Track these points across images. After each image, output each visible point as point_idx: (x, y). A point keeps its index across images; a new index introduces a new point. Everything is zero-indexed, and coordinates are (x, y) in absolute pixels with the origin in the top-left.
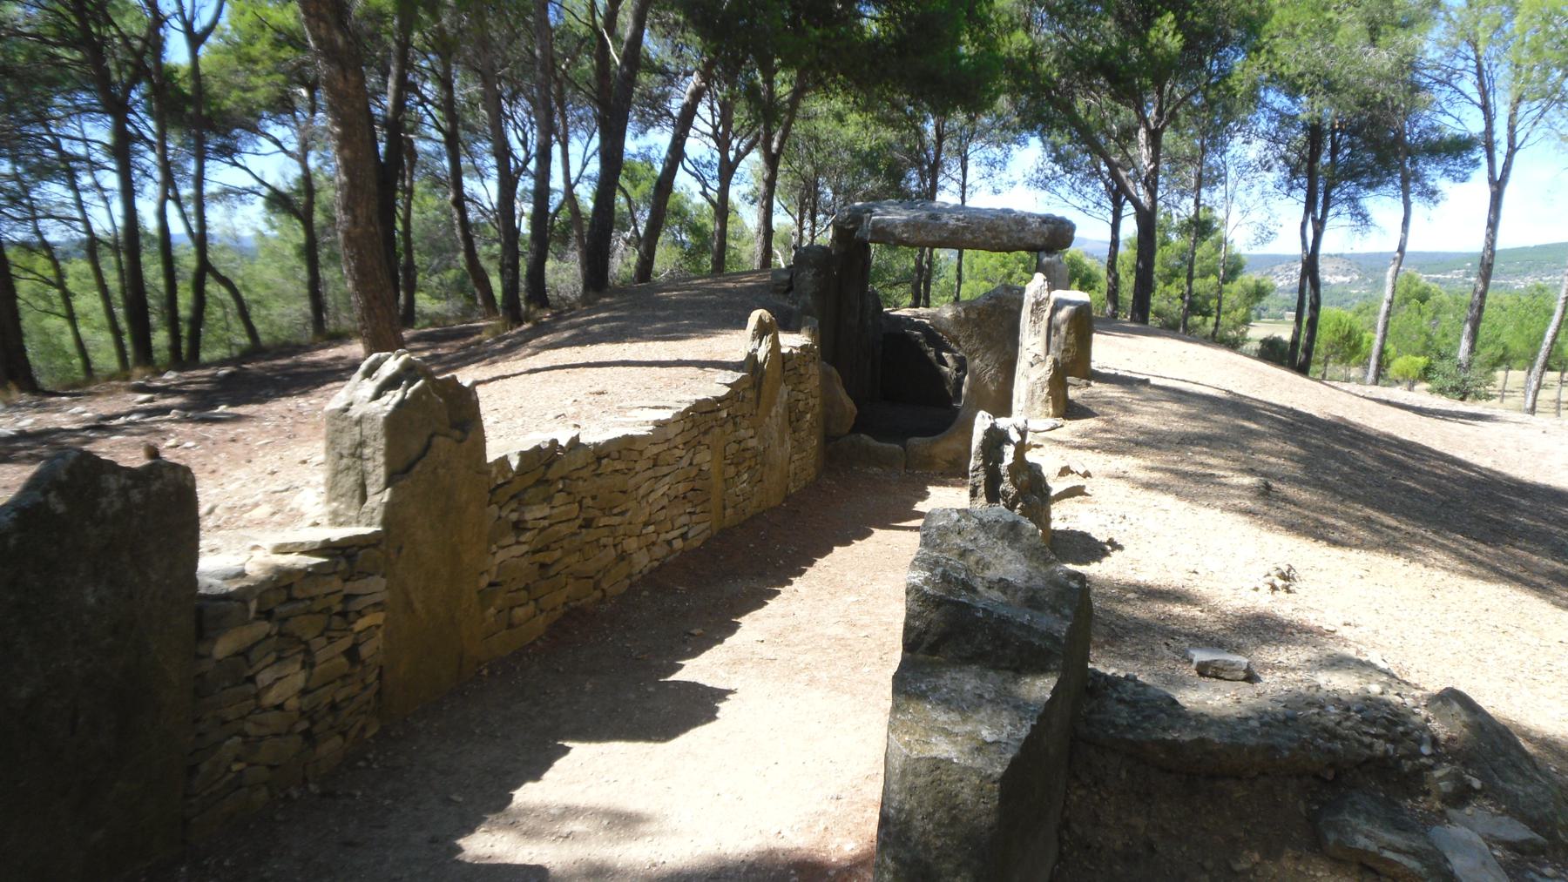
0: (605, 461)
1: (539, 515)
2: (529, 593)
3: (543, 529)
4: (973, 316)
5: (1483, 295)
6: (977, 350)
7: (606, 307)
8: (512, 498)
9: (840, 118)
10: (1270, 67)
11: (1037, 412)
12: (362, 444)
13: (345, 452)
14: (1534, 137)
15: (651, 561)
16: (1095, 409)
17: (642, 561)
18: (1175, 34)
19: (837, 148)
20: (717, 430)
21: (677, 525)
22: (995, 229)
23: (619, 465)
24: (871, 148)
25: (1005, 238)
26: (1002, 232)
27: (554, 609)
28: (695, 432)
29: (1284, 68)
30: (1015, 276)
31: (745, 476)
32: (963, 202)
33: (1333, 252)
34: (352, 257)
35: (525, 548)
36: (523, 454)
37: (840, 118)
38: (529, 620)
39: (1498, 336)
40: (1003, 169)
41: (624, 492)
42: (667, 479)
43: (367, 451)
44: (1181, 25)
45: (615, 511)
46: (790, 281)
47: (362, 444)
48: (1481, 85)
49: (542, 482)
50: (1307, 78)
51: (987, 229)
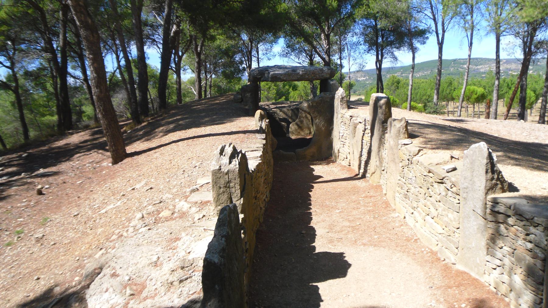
4: (315, 104)
5: (439, 81)
6: (317, 116)
10: (367, 10)
12: (229, 182)
13: (222, 186)
14: (449, 27)
22: (315, 73)
24: (226, 48)
26: (317, 74)
30: (271, 88)
34: (101, 106)
43: (232, 185)
47: (229, 182)
48: (433, 12)
51: (312, 74)
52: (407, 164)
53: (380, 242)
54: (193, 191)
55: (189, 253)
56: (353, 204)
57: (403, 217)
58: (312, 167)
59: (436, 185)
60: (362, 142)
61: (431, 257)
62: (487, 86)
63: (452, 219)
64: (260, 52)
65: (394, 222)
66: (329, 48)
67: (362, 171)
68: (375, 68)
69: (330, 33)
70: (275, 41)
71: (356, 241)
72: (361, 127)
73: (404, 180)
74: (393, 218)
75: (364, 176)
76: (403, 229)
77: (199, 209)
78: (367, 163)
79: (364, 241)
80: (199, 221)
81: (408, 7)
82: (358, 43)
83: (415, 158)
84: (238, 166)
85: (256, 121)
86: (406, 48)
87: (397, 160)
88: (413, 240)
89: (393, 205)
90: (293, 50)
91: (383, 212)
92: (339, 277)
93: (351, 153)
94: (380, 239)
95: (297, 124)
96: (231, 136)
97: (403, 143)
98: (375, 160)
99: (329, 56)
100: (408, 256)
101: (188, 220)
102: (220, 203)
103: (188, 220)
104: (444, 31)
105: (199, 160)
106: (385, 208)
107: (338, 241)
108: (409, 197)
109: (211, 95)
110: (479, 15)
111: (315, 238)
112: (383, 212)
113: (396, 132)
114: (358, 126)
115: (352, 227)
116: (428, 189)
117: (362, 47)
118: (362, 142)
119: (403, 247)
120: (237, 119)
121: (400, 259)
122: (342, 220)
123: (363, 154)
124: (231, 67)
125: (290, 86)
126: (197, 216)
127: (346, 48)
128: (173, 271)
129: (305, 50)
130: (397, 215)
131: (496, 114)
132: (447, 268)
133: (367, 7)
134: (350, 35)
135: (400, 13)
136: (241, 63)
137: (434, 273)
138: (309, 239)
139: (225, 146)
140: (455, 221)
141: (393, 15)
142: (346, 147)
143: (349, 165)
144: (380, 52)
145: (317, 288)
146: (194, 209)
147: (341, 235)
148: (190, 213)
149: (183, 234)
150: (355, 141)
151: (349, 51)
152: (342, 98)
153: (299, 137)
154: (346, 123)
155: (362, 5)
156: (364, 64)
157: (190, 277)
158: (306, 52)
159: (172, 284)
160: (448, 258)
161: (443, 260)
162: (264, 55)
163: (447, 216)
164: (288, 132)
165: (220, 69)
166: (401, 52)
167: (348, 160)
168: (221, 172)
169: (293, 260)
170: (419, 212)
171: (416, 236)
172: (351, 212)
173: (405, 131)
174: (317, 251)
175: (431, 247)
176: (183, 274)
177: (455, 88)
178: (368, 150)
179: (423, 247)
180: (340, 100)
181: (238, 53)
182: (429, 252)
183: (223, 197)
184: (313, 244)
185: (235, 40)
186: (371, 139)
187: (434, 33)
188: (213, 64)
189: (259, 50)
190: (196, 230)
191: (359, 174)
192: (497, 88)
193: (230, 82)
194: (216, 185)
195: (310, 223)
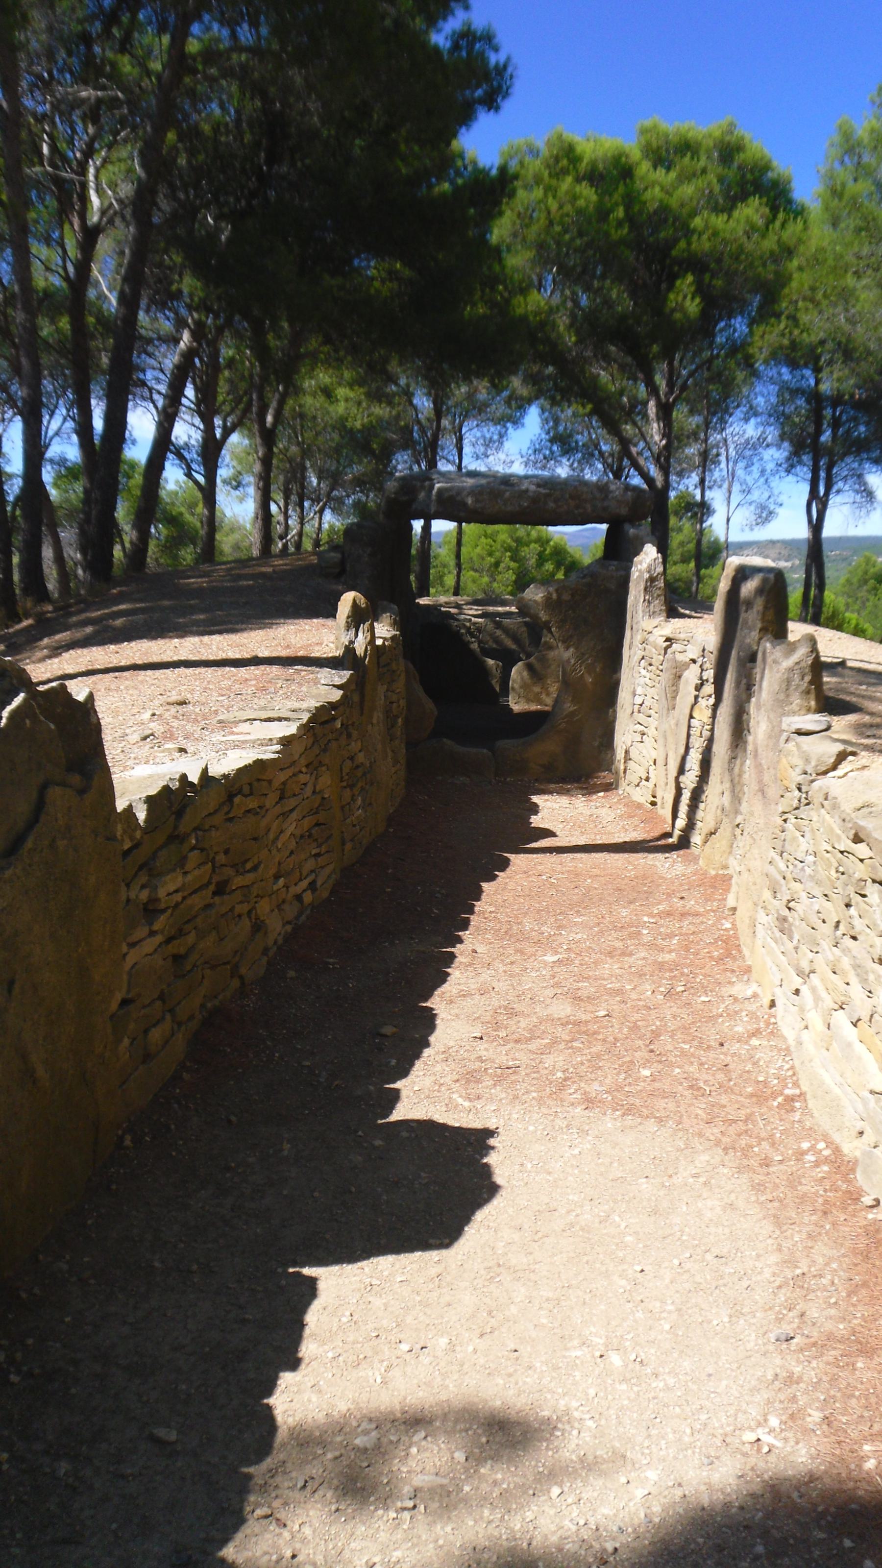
0: (237, 800)
1: (172, 888)
2: (164, 1002)
3: (177, 905)
4: (566, 597)
6: (571, 636)
7: (121, 598)
8: (141, 868)
9: (328, 393)
10: (791, 333)
11: (794, 707)
15: (284, 925)
17: (276, 927)
18: (693, 299)
19: (324, 428)
20: (334, 745)
21: (304, 874)
23: (252, 803)
24: (363, 425)
25: (589, 508)
27: (192, 1017)
28: (316, 750)
29: (805, 335)
30: (502, 565)
31: (359, 801)
35: (159, 939)
36: (149, 800)
37: (328, 393)
38: (166, 1042)
41: (255, 839)
42: (294, 815)
44: (701, 290)
45: (249, 866)
46: (342, 562)
49: (175, 838)
50: (830, 345)
52: (795, 803)
57: (766, 1002)
60: (689, 727)
61: (827, 1184)
64: (467, 450)
65: (732, 1015)
66: (667, 447)
67: (681, 823)
72: (691, 675)
74: (736, 1000)
75: (684, 843)
76: (755, 1048)
79: (596, 1086)
82: (761, 442)
83: (822, 782)
89: (746, 952)
91: (705, 975)
92: (425, 1246)
94: (657, 1085)
95: (530, 668)
99: (665, 470)
108: (791, 930)
111: (418, 1056)
112: (705, 975)
113: (777, 687)
115: (577, 1023)
116: (848, 905)
119: (732, 1130)
121: (702, 1180)
122: (550, 992)
123: (687, 767)
129: (601, 454)
133: (790, 322)
134: (739, 413)
137: (821, 1260)
138: (393, 1062)
141: (869, 353)
143: (653, 804)
144: (823, 474)
150: (673, 722)
151: (731, 464)
152: (652, 580)
153: (534, 707)
154: (653, 661)
155: (778, 316)
156: (772, 507)
162: (478, 458)
164: (505, 690)
167: (650, 784)
170: (813, 990)
171: (796, 1084)
173: (811, 683)
175: (837, 1137)
180: (642, 587)
186: (714, 716)
189: (466, 442)
191: (669, 835)
195: (428, 996)
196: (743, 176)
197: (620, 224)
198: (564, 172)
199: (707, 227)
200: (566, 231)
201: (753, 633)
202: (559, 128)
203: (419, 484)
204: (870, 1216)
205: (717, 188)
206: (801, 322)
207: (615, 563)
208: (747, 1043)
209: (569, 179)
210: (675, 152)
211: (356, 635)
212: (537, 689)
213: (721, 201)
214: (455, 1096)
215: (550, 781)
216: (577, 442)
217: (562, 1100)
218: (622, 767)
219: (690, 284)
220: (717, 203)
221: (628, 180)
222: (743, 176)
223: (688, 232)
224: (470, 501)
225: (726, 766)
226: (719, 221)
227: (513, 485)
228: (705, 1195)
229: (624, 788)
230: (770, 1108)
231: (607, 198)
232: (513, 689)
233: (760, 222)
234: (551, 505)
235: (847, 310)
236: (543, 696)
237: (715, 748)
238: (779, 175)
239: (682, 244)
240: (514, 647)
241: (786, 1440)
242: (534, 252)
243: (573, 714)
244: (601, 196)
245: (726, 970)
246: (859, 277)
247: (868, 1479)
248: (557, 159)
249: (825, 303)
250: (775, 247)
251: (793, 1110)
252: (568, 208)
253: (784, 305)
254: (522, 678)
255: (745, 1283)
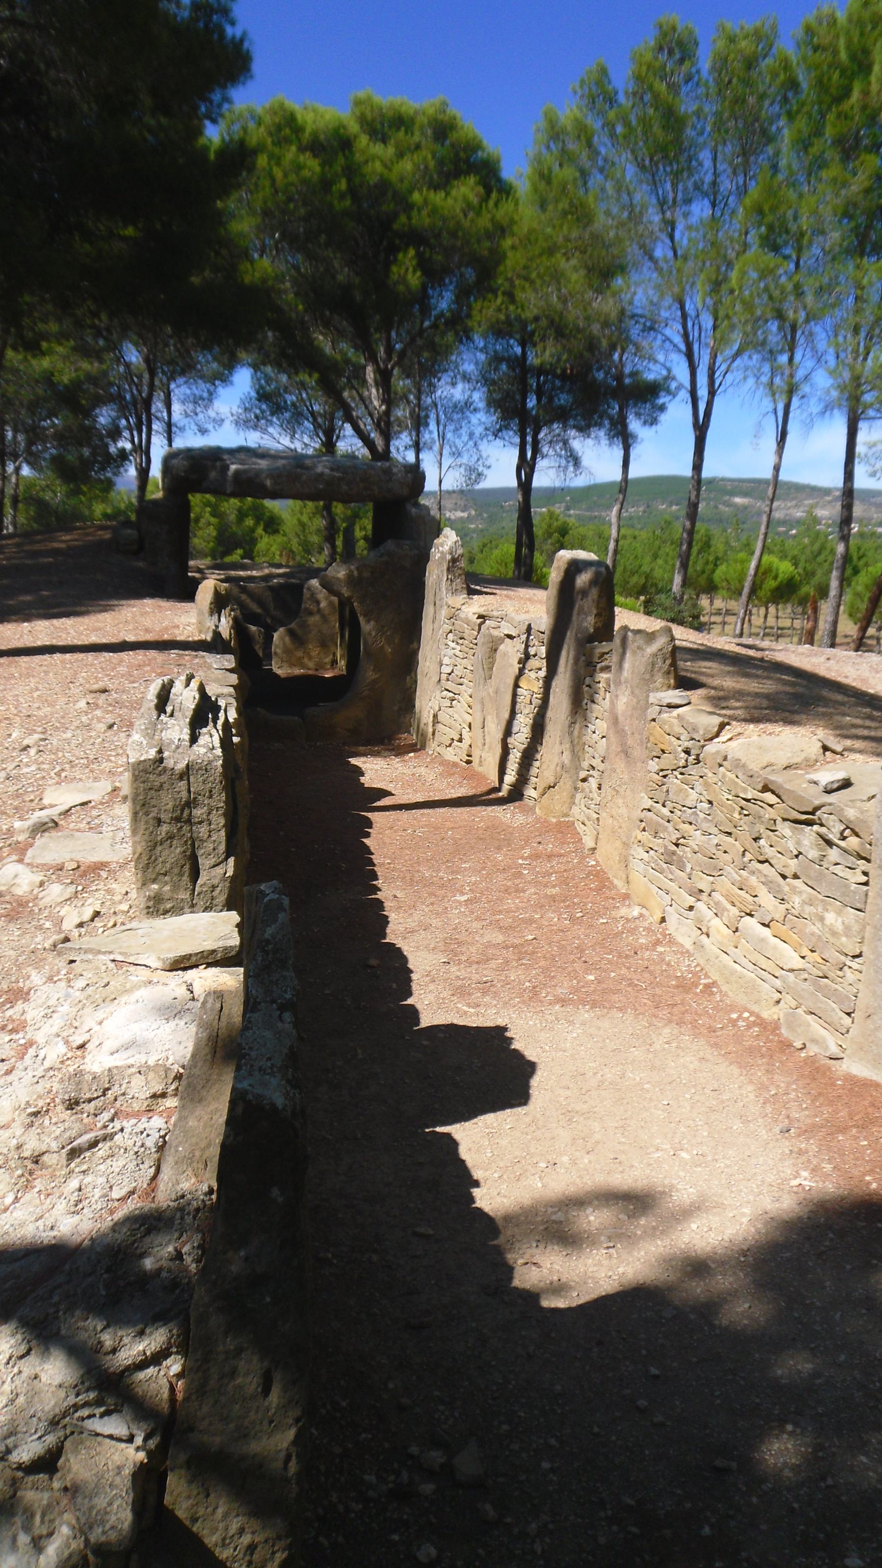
4: (366, 574)
10: (507, 309)
11: (658, 684)
12: (190, 804)
16: (703, 679)
18: (414, 271)
30: (203, 521)
32: (698, 466)
33: (450, 489)
39: (640, 566)
40: (206, 407)
44: (423, 265)
47: (190, 804)
48: (686, 336)
52: (682, 763)
53: (604, 992)
54: (41, 828)
55: (82, 1046)
56: (501, 876)
57: (658, 916)
58: (353, 761)
59: (785, 829)
60: (515, 695)
62: (803, 558)
63: (839, 927)
64: (176, 407)
66: (387, 413)
67: (510, 778)
68: (514, 483)
69: (393, 368)
70: (223, 377)
71: (535, 992)
72: (512, 651)
73: (665, 811)
74: (628, 920)
75: (516, 794)
76: (661, 953)
77: (72, 889)
78: (528, 756)
80: (83, 930)
81: (622, 312)
82: (467, 406)
83: (711, 748)
84: (219, 752)
85: (200, 613)
86: (602, 433)
87: (637, 752)
88: (701, 987)
90: (277, 409)
92: (512, 1106)
93: (477, 726)
95: (292, 633)
96: (124, 655)
97: (665, 702)
98: (557, 748)
100: (696, 1035)
101: (40, 928)
102: (159, 874)
103: (40, 928)
104: (712, 393)
105: (31, 727)
106: (599, 890)
107: (485, 993)
109: (15, 526)
110: (809, 354)
111: (410, 980)
114: (502, 647)
115: (515, 947)
116: (756, 839)
117: (478, 416)
118: (515, 695)
119: (675, 1009)
120: (124, 602)
121: (674, 1045)
123: (515, 729)
124: (82, 446)
125: (258, 519)
126: (71, 917)
127: (433, 416)
128: (36, 1114)
129: (312, 413)
130: (636, 911)
131: (833, 634)
132: (817, 1069)
133: (505, 299)
134: (446, 378)
135: (599, 326)
136: (115, 433)
138: (394, 986)
139: (171, 683)
140: (847, 936)
141: (578, 330)
142: (461, 706)
143: (469, 762)
144: (529, 439)
145: (451, 1144)
146: (56, 891)
147: (488, 974)
148: (42, 904)
149: (36, 978)
150: (491, 690)
151: (441, 428)
152: (454, 561)
153: (298, 671)
155: (494, 292)
156: (480, 469)
157: (104, 1139)
158: (315, 419)
159: (37, 1162)
160: (814, 1041)
161: (800, 1046)
163: (822, 919)
164: (269, 657)
165: (46, 449)
166: (590, 442)
167: (465, 745)
168: (165, 769)
169: (360, 1051)
171: (707, 976)
172: (501, 900)
173: (671, 665)
174: (426, 1021)
175: (755, 1008)
176: (77, 1127)
177: (717, 559)
178: (535, 719)
179: (732, 1008)
180: (445, 567)
181: (105, 404)
182: (754, 1024)
183: (166, 852)
184: (409, 1001)
185: (101, 361)
187: (684, 395)
188: (26, 431)
189: (174, 399)
190: (85, 965)
191: (499, 790)
192: (840, 562)
193: (76, 492)
194: (147, 814)
196: (457, 154)
197: (342, 196)
198: (287, 141)
199: (426, 201)
200: (290, 199)
201: (589, 618)
202: (280, 96)
203: (209, 463)
204: (803, 1055)
205: (432, 164)
206: (517, 298)
207: (408, 542)
208: (654, 950)
209: (293, 148)
210: (390, 127)
211: (219, 620)
212: (300, 654)
213: (435, 176)
214: (459, 1005)
215: (357, 744)
216: (286, 402)
217: (541, 1001)
218: (431, 730)
219: (412, 258)
220: (431, 178)
221: (347, 152)
222: (457, 154)
223: (409, 207)
224: (268, 483)
225: (567, 729)
226: (437, 198)
227: (307, 468)
228: (682, 1054)
229: (432, 747)
230: (696, 994)
231: (327, 168)
232: (276, 653)
233: (475, 201)
234: (345, 487)
235: (559, 290)
236: (306, 660)
237: (550, 714)
238: (489, 154)
239: (403, 219)
240: (259, 611)
241: (817, 1182)
242: (259, 219)
243: (375, 681)
244: (323, 165)
245: (607, 898)
246: (568, 259)
247: (876, 1193)
248: (279, 128)
249: (538, 282)
250: (489, 225)
251: (712, 993)
252: (293, 178)
253: (500, 281)
254: (284, 644)
255: (741, 1104)
